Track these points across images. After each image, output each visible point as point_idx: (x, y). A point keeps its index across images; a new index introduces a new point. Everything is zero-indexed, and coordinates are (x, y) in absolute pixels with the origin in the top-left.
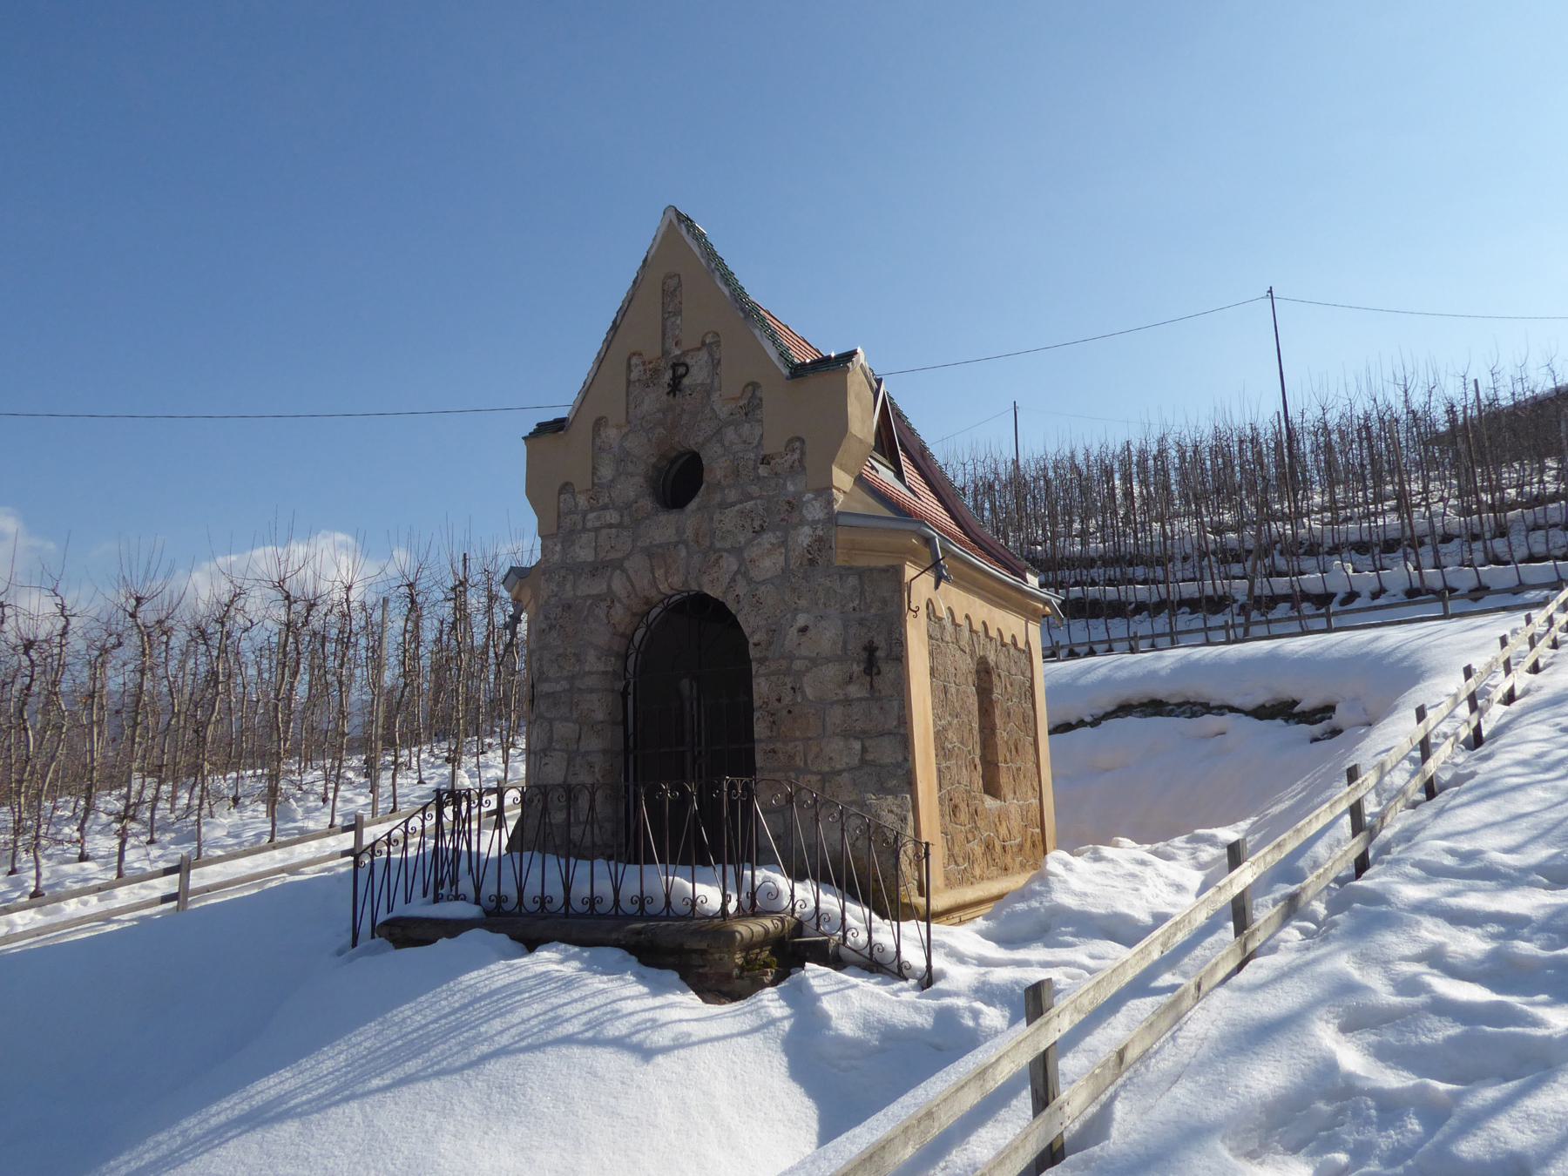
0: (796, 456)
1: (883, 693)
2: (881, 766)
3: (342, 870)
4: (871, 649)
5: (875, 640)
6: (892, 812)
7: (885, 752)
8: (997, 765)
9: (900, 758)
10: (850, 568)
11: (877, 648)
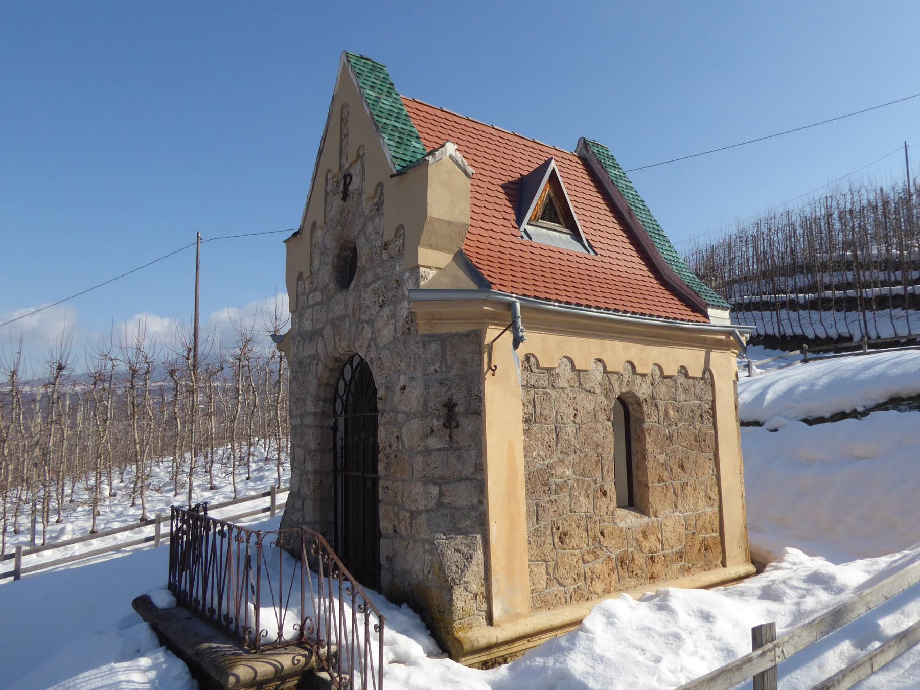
0: (401, 242)
1: (461, 443)
2: (457, 508)
3: (265, 520)
4: (450, 406)
5: (454, 397)
6: (458, 551)
7: (462, 496)
8: (647, 485)
9: (475, 501)
10: (433, 336)
11: (456, 405)
